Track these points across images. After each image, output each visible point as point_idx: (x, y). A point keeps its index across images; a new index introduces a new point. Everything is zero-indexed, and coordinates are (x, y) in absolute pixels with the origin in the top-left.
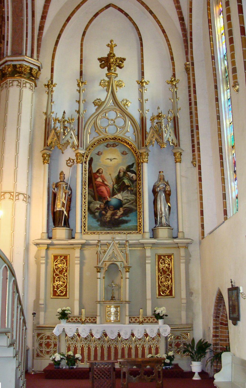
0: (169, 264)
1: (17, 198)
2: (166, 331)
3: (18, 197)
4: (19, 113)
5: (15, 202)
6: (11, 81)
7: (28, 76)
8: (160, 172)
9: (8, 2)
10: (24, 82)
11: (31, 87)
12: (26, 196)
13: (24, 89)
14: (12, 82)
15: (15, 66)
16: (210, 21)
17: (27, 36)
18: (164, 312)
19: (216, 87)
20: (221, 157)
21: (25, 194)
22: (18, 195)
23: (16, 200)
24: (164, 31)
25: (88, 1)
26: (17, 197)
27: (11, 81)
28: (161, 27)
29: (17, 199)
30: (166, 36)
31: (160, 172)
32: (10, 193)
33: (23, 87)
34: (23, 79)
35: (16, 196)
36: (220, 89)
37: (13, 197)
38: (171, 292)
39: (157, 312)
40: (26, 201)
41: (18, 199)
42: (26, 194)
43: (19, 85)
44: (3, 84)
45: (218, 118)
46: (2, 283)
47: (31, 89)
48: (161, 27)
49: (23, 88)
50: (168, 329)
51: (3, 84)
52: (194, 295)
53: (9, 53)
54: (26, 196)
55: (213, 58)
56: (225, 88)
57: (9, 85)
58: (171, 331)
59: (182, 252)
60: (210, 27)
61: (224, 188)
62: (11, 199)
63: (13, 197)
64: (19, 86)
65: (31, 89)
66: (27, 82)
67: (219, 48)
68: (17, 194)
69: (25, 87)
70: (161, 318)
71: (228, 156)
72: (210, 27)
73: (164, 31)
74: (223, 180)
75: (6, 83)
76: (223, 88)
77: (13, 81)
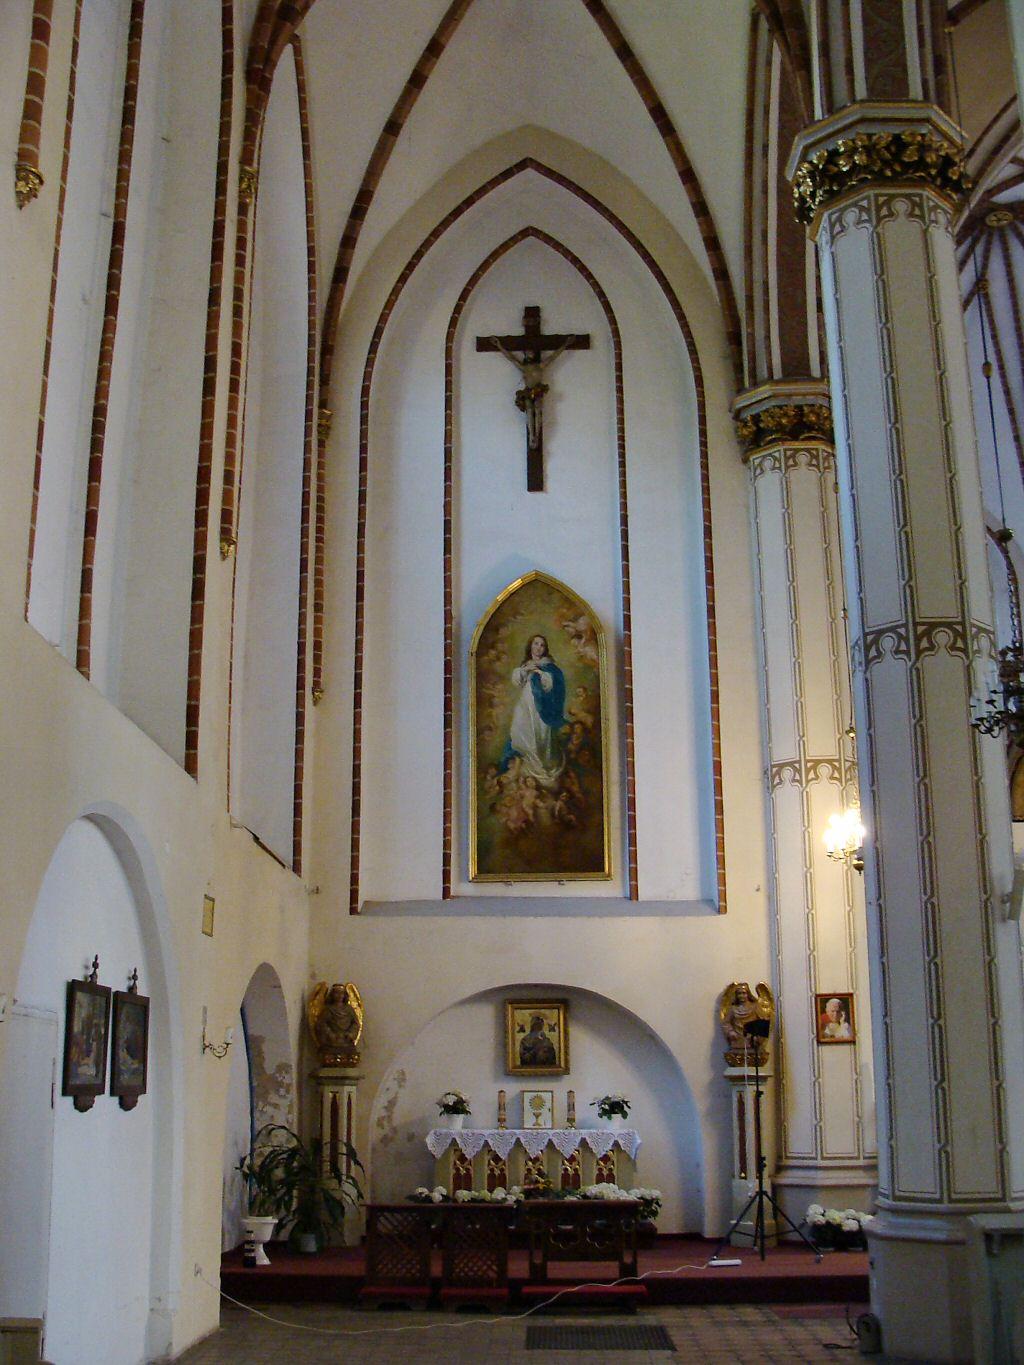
2: (954, 174)
4: (892, 378)
11: (959, 640)
37: (840, 774)
43: (903, 647)
46: (788, 1279)
49: (807, 785)
63: (840, 774)
64: (903, 652)
69: (891, 214)
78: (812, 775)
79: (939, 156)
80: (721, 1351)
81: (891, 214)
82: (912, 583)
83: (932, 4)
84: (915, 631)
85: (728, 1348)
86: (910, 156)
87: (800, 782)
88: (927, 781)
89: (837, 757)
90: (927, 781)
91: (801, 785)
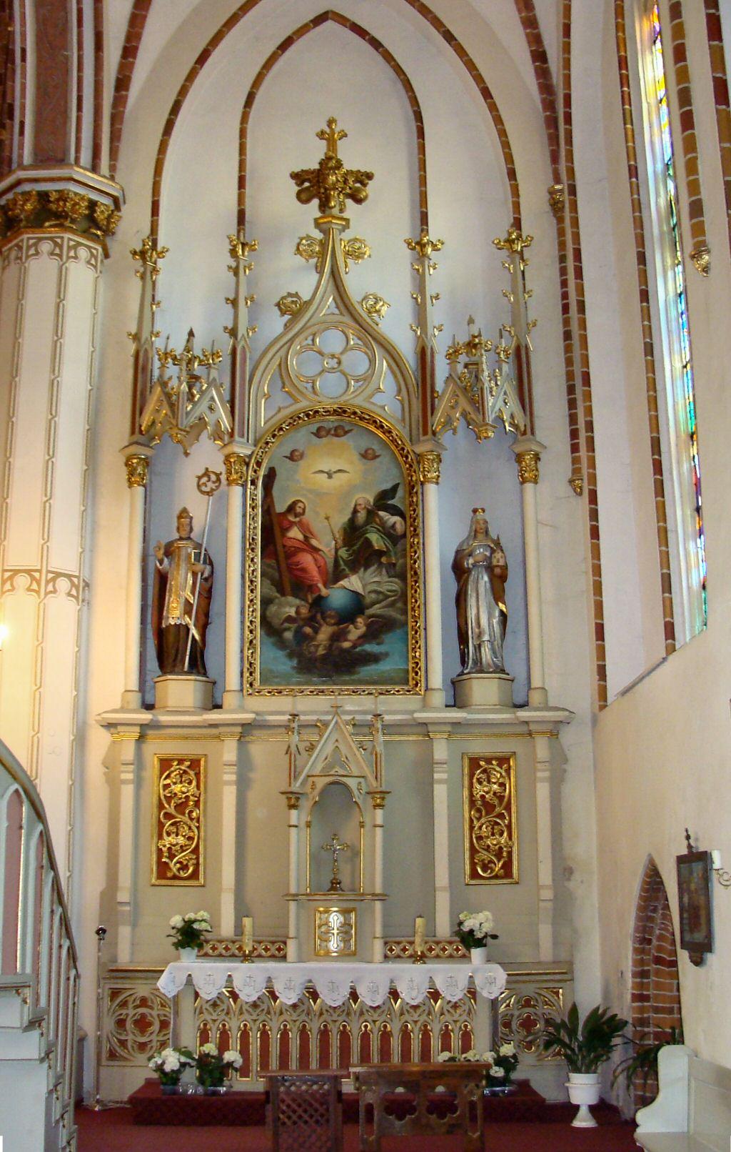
0: (502, 785)
1: (50, 588)
2: (492, 982)
3: (54, 586)
4: (57, 336)
5: (45, 601)
6: (31, 242)
7: (85, 225)
8: (475, 511)
9: (23, 6)
10: (72, 243)
12: (76, 583)
13: (71, 265)
14: (35, 245)
15: (44, 196)
16: (623, 63)
17: (80, 108)
18: (487, 927)
19: (642, 258)
20: (658, 467)
21: (75, 576)
22: (53, 580)
23: (46, 594)
24: (486, 93)
25: (260, 4)
26: (51, 585)
27: (31, 242)
28: (478, 79)
29: (51, 592)
30: (493, 108)
31: (475, 511)
32: (28, 572)
33: (68, 258)
34: (67, 236)
35: (47, 582)
36: (655, 264)
37: (39, 585)
38: (508, 866)
39: (466, 928)
40: (77, 598)
41: (55, 591)
42: (78, 577)
43: (57, 251)
44: (10, 249)
45: (649, 349)
46: (7, 841)
47: (92, 265)
48: (478, 79)
49: (67, 260)
50: (501, 975)
51: (10, 249)
52: (577, 876)
53: (27, 159)
54: (76, 583)
55: (633, 172)
56: (669, 261)
57: (27, 253)
58: (508, 982)
59: (542, 748)
60: (624, 81)
61: (665, 560)
62: (33, 590)
63: (39, 585)
64: (57, 255)
65: (92, 265)
66: (79, 244)
67: (652, 143)
68: (50, 576)
69: (76, 257)
70: (480, 943)
71: (679, 462)
72: (624, 81)
73: (486, 93)
74: (663, 535)
75: (17, 245)
76: (663, 260)
77: (40, 239)
78: (32, 251)
79: (57, 209)
80: (288, 1106)
81: (76, 257)
82: (50, 417)
83: (39, 3)
84: (47, 576)
85: (693, 418)
86: (132, 1036)
87: (60, 256)
88: (56, 338)
89: (39, 568)
90: (56, 338)
91: (62, 260)
